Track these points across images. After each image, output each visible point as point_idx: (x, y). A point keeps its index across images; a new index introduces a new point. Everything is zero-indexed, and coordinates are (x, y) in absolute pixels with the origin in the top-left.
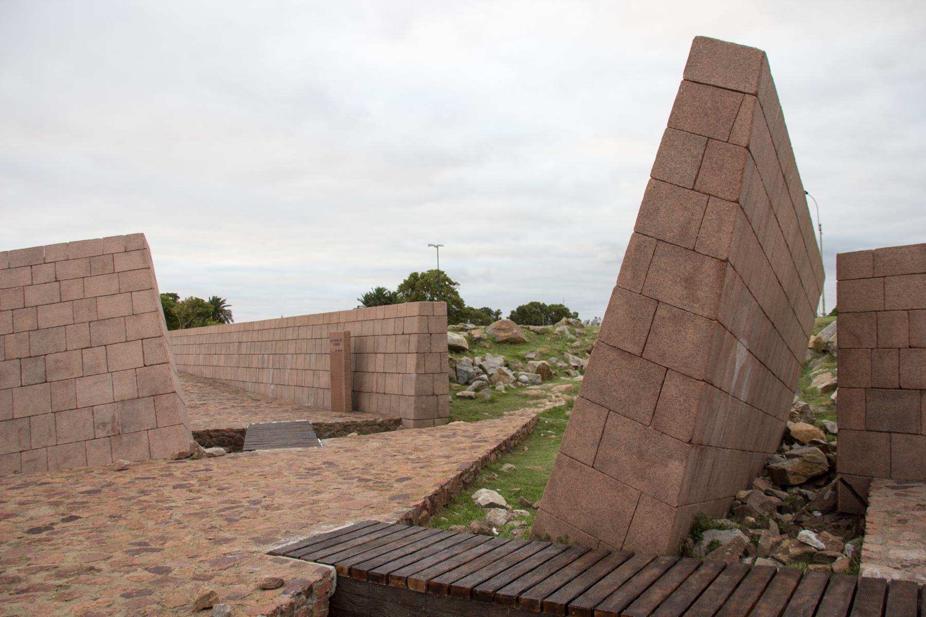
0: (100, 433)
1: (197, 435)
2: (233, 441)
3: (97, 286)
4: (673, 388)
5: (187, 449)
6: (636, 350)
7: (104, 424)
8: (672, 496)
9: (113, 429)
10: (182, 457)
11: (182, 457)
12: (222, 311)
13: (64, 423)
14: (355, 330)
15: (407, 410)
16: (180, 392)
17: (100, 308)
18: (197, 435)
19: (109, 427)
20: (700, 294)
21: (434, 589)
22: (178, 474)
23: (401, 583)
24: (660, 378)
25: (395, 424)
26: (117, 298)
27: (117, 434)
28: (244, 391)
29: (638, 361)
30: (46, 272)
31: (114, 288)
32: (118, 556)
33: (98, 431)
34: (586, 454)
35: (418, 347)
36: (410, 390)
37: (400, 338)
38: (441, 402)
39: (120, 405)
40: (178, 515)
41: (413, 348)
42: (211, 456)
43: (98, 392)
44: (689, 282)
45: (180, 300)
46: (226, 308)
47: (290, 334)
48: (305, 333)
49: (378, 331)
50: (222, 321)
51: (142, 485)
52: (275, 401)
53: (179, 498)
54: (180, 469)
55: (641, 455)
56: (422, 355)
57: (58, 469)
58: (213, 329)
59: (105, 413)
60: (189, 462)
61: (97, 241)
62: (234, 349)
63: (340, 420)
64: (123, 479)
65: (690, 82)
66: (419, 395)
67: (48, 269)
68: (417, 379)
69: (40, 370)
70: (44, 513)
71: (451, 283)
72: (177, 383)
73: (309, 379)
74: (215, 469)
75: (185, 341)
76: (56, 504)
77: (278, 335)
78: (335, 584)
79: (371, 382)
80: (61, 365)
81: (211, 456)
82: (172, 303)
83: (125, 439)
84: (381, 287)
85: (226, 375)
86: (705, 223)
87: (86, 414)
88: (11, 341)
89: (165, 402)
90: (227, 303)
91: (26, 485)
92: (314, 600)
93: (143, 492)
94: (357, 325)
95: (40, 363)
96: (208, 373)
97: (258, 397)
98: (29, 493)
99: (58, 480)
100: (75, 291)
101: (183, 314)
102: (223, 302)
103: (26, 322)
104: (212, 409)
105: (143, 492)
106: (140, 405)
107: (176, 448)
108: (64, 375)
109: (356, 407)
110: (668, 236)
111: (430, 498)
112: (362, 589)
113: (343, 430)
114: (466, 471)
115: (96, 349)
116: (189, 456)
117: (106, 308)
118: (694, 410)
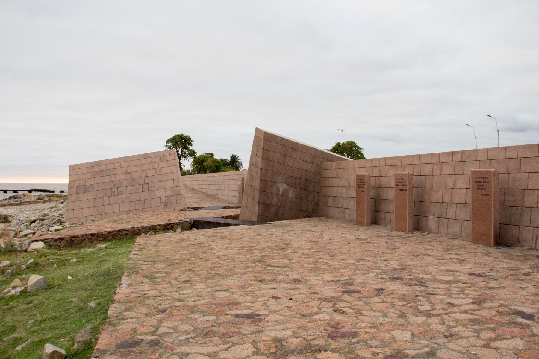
0: (162, 205)
3: (162, 164)
13: (153, 202)
21: (204, 222)
27: (166, 205)
30: (148, 160)
43: (162, 194)
44: (257, 172)
52: (224, 201)
59: (163, 199)
61: (162, 151)
67: (149, 159)
69: (147, 187)
71: (359, 148)
85: (214, 193)
87: (159, 199)
88: (140, 179)
89: (179, 197)
90: (240, 158)
100: (156, 166)
102: (238, 157)
103: (143, 174)
106: (172, 197)
108: (153, 189)
117: (164, 171)
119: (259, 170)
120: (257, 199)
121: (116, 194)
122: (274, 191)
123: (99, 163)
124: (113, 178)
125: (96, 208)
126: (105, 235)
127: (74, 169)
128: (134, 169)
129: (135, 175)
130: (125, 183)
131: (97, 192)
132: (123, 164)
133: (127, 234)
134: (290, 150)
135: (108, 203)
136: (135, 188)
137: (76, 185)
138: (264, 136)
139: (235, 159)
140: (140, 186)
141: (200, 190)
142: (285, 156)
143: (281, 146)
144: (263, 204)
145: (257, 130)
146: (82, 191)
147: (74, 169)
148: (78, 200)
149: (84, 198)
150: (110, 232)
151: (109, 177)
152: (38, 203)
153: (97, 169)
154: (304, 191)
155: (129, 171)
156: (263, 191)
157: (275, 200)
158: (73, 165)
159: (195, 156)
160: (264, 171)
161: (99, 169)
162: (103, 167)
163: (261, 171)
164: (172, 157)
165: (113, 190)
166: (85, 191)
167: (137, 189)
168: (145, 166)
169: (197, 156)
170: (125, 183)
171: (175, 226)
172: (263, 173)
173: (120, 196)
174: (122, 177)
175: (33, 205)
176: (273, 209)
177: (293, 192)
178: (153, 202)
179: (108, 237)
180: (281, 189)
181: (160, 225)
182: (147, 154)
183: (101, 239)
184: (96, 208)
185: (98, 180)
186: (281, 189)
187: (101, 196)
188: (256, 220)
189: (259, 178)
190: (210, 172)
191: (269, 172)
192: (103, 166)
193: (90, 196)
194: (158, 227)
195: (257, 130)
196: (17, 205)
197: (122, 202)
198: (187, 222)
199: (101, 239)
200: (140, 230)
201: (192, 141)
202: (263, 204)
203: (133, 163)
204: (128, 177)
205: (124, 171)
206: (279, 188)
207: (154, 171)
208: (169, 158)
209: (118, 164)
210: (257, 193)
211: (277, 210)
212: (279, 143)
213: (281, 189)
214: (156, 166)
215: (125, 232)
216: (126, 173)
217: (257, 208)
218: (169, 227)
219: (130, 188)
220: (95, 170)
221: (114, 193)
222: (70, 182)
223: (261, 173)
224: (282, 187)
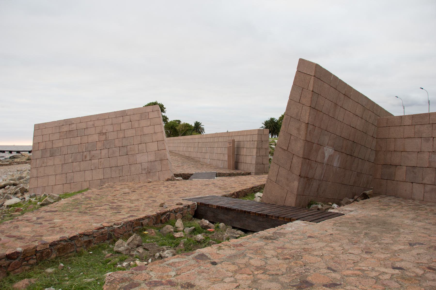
0: (144, 172)
1: (174, 174)
2: (186, 177)
3: (144, 123)
4: (295, 160)
5: (170, 178)
6: (286, 148)
7: (145, 169)
8: (295, 192)
9: (148, 171)
10: (168, 180)
11: (168, 180)
12: (200, 128)
13: (133, 168)
14: (237, 139)
15: (252, 169)
16: (170, 159)
17: (144, 130)
18: (174, 174)
19: (147, 170)
20: (301, 133)
21: (218, 207)
22: (166, 184)
23: (211, 206)
24: (292, 157)
25: (249, 174)
26: (150, 127)
27: (149, 172)
28: (199, 161)
29: (286, 152)
30: (127, 118)
31: (149, 124)
32: (145, 198)
33: (143, 171)
34: (274, 179)
35: (257, 146)
36: (254, 162)
37: (252, 142)
38: (266, 167)
39: (150, 163)
40: (162, 192)
41: (255, 147)
42: (178, 180)
43: (143, 159)
44: (298, 129)
45: (181, 123)
46: (202, 127)
47: (216, 140)
48: (221, 139)
49: (245, 140)
50: (200, 133)
51: (154, 186)
52: (210, 165)
53: (164, 189)
54: (166, 183)
55: (287, 179)
56: (258, 149)
57: (131, 181)
58: (196, 136)
59: (145, 165)
60: (170, 181)
62: (196, 145)
63: (228, 172)
64: (148, 185)
65: (299, 72)
66: (257, 164)
67: (128, 117)
68: (256, 158)
70: (127, 190)
72: (169, 156)
73: (221, 157)
74: (177, 183)
75: (179, 141)
76: (130, 189)
77: (212, 140)
78: (196, 206)
79: (242, 159)
80: (132, 149)
81: (178, 180)
82: (178, 125)
83: (151, 174)
84: (272, 117)
85: (193, 155)
86: (302, 113)
87: (139, 165)
89: (164, 162)
91: (122, 185)
92: (189, 209)
93: (154, 187)
94: (238, 137)
95: (125, 149)
96: (187, 154)
97: (204, 164)
98: (123, 186)
99: (131, 184)
101: (181, 130)
103: (121, 135)
104: (185, 167)
105: (154, 187)
106: (156, 163)
107: (167, 177)
108: (133, 153)
109: (236, 168)
110: (293, 116)
111: (236, 192)
112: (203, 208)
113: (230, 175)
114: (255, 187)
115: (143, 144)
116: (171, 180)
117: (147, 130)
118: (300, 167)
119: (303, 126)
120: (297, 171)
121: (88, 158)
122: (319, 159)
124: (85, 139)
126: (42, 252)
127: (38, 128)
128: (110, 128)
129: (111, 136)
130: (99, 145)
131: (66, 156)
132: (97, 123)
133: (90, 242)
134: (342, 96)
135: (78, 169)
136: (111, 151)
137: (42, 147)
138: (315, 72)
140: (117, 149)
141: (176, 152)
142: (336, 104)
144: (304, 177)
145: (302, 62)
146: (48, 154)
147: (38, 128)
148: (43, 165)
149: (50, 163)
150: (53, 244)
151: (80, 138)
152: (26, 163)
153: (66, 129)
154: (349, 157)
155: (104, 131)
156: (306, 158)
157: (318, 172)
158: (39, 124)
159: (166, 121)
160: (311, 127)
161: (68, 129)
162: (74, 127)
163: (307, 127)
164: (155, 114)
165: (85, 153)
168: (122, 125)
169: (169, 121)
170: (99, 145)
171: (173, 215)
172: (309, 129)
173: (93, 161)
174: (96, 138)
175: (21, 165)
176: (315, 184)
177: (339, 158)
178: (133, 168)
179: (48, 254)
180: (327, 155)
181: (148, 217)
183: (31, 262)
185: (67, 142)
186: (327, 155)
187: (70, 161)
188: (293, 205)
189: (303, 138)
190: (182, 135)
191: (317, 128)
192: (73, 126)
193: (58, 160)
194: (146, 221)
195: (302, 62)
196: (6, 165)
197: (95, 168)
198: (189, 206)
199: (31, 262)
200: (114, 230)
201: (165, 108)
202: (304, 177)
203: (109, 122)
204: (103, 138)
205: (98, 131)
206: (324, 154)
207: (133, 131)
208: (151, 115)
209: (92, 123)
210: (297, 162)
211: (319, 185)
213: (326, 154)
214: (136, 125)
215: (86, 239)
216: (101, 133)
217: (296, 183)
218: (163, 218)
219: (104, 152)
220: (63, 130)
221: (86, 157)
222: (34, 144)
223: (307, 131)
224: (328, 151)
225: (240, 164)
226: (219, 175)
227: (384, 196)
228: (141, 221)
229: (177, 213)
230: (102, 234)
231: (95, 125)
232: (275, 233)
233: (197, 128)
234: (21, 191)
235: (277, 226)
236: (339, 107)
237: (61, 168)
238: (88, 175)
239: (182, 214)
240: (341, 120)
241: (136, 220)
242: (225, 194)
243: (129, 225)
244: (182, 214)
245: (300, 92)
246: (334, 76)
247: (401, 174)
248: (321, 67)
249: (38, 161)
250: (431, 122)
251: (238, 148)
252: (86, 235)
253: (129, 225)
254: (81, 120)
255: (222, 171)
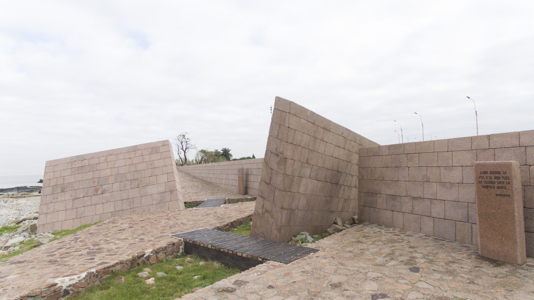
3: (155, 157)
79: (251, 185)
96: (208, 180)
103: (133, 169)
109: (246, 193)
110: (273, 151)
113: (242, 200)
117: (157, 164)
121: (100, 192)
123: (81, 158)
125: (75, 210)
134: (322, 130)
135: (89, 203)
139: (228, 153)
143: (311, 124)
144: (287, 209)
145: (278, 100)
146: (59, 190)
148: (54, 201)
162: (86, 163)
166: (62, 191)
167: (125, 186)
174: (108, 172)
182: (137, 146)
184: (75, 210)
185: (79, 177)
187: (82, 196)
193: (67, 196)
195: (278, 100)
202: (287, 209)
209: (103, 158)
212: (309, 119)
225: (248, 189)
226: (230, 201)
227: (368, 223)
228: (111, 269)
229: (159, 252)
230: (55, 291)
231: (108, 160)
232: (236, 283)
233: (226, 154)
234: (31, 228)
235: (244, 271)
236: (319, 141)
237: (71, 203)
238: (99, 209)
239: (165, 253)
240: (323, 152)
241: (104, 268)
242: (219, 225)
243: (94, 276)
244: (165, 253)
245: (278, 128)
246: (311, 111)
247: (381, 202)
248: (296, 104)
249: (48, 197)
250: (406, 153)
251: (247, 175)
252: (31, 297)
253: (94, 276)
254: (93, 156)
255: (233, 197)
